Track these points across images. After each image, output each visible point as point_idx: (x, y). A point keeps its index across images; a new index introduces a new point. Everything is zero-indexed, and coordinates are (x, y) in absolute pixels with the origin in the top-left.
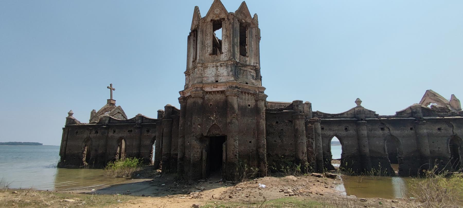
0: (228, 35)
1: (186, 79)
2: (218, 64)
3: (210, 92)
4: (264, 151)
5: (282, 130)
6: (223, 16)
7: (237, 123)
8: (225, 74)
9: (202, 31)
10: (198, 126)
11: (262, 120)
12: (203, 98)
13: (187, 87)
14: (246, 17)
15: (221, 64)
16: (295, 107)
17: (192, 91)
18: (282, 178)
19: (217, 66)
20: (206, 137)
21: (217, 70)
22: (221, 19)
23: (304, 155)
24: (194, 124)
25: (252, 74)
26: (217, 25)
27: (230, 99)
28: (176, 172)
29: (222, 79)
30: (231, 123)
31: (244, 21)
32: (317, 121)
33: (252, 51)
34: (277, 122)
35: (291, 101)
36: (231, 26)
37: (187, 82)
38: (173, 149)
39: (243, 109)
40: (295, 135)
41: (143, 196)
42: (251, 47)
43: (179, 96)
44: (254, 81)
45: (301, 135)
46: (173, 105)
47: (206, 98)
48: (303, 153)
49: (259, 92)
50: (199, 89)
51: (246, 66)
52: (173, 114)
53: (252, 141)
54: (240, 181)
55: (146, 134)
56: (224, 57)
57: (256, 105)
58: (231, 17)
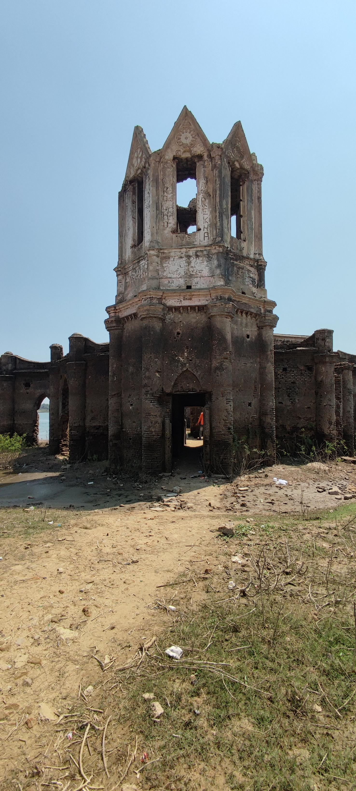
0: (211, 191)
1: (119, 282)
2: (192, 252)
3: (177, 309)
4: (271, 421)
5: (293, 383)
6: (199, 149)
7: (233, 368)
8: (206, 272)
9: (156, 180)
10: (156, 374)
11: (270, 364)
12: (163, 320)
13: (121, 299)
14: (242, 157)
15: (197, 252)
16: (320, 341)
17: (142, 306)
18: (304, 467)
19: (189, 257)
20: (168, 394)
21: (189, 263)
22: (194, 156)
23: (332, 426)
24: (148, 369)
25: (252, 275)
26: (186, 169)
27: (218, 322)
28: (107, 459)
29: (200, 283)
30: (220, 368)
31: (237, 165)
32: (348, 368)
33: (252, 229)
34: (285, 369)
35: (310, 333)
36: (216, 172)
37: (122, 289)
38: (88, 418)
39: (238, 342)
40: (316, 393)
41: (71, 507)
42: (251, 221)
43: (107, 316)
44: (254, 290)
45: (328, 392)
46: (85, 335)
47: (168, 321)
48: (330, 423)
49: (267, 311)
50: (155, 301)
51: (242, 258)
52: (86, 352)
53: (253, 403)
54: (238, 474)
55: (23, 390)
56: (202, 238)
57: (260, 335)
58: (216, 153)
